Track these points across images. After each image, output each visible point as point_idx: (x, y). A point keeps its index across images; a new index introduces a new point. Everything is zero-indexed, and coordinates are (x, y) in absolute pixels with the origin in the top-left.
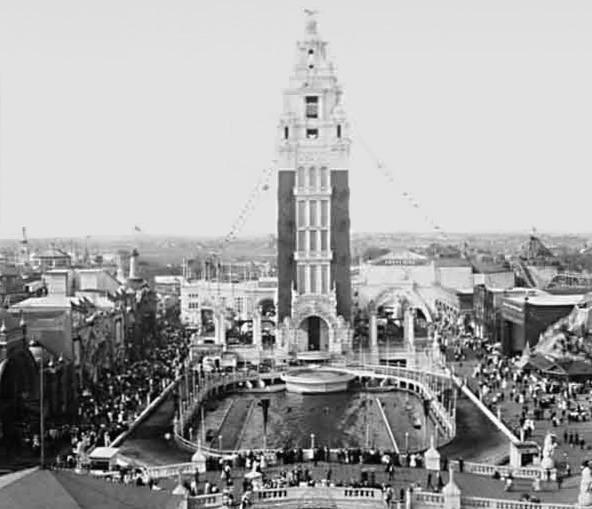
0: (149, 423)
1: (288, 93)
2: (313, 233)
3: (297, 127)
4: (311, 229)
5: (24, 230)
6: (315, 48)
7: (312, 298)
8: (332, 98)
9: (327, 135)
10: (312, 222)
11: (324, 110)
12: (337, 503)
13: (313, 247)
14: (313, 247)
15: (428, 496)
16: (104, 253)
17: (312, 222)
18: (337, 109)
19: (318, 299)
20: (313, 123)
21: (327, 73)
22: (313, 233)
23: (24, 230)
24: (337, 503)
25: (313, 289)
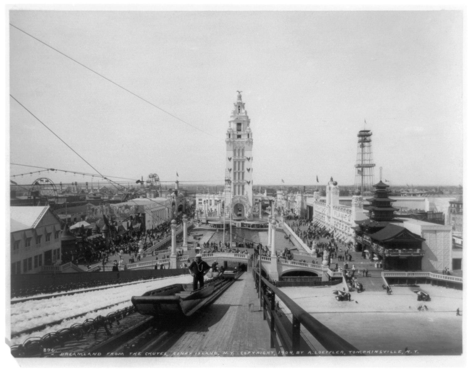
0: (163, 305)
1: (230, 122)
2: (239, 173)
3: (233, 134)
4: (239, 171)
5: (365, 137)
6: (240, 106)
7: (238, 197)
8: (246, 123)
9: (244, 138)
10: (239, 169)
11: (243, 128)
12: (93, 185)
13: (239, 178)
14: (239, 178)
15: (282, 260)
16: (147, 213)
17: (239, 169)
18: (248, 128)
19: (240, 197)
20: (239, 133)
21: (244, 115)
22: (239, 173)
23: (365, 137)
24: (93, 185)
25: (239, 193)
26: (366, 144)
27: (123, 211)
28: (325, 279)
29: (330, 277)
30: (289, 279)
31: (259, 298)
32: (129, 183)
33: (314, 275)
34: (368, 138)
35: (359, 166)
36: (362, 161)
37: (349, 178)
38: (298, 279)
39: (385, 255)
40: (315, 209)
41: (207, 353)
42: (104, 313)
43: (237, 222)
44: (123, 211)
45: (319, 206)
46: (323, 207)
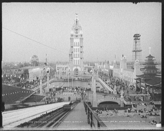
23: (137, 37)
26: (137, 41)
27: (18, 72)
28: (122, 106)
29: (125, 104)
30: (103, 106)
31: (86, 114)
32: (134, 45)
33: (117, 103)
34: (139, 38)
35: (134, 51)
36: (136, 49)
37: (130, 56)
38: (108, 106)
39: (154, 93)
40: (114, 72)
41: (112, 126)
42: (54, 110)
43: (76, 78)
44: (18, 72)
45: (116, 69)
46: (118, 70)
